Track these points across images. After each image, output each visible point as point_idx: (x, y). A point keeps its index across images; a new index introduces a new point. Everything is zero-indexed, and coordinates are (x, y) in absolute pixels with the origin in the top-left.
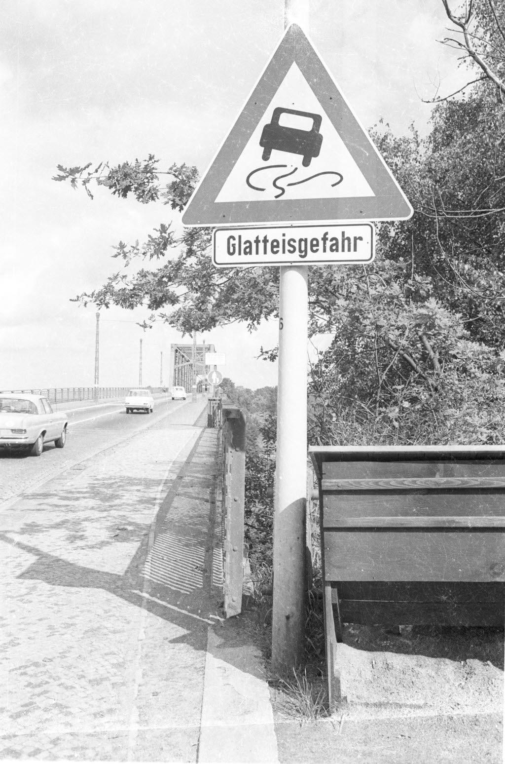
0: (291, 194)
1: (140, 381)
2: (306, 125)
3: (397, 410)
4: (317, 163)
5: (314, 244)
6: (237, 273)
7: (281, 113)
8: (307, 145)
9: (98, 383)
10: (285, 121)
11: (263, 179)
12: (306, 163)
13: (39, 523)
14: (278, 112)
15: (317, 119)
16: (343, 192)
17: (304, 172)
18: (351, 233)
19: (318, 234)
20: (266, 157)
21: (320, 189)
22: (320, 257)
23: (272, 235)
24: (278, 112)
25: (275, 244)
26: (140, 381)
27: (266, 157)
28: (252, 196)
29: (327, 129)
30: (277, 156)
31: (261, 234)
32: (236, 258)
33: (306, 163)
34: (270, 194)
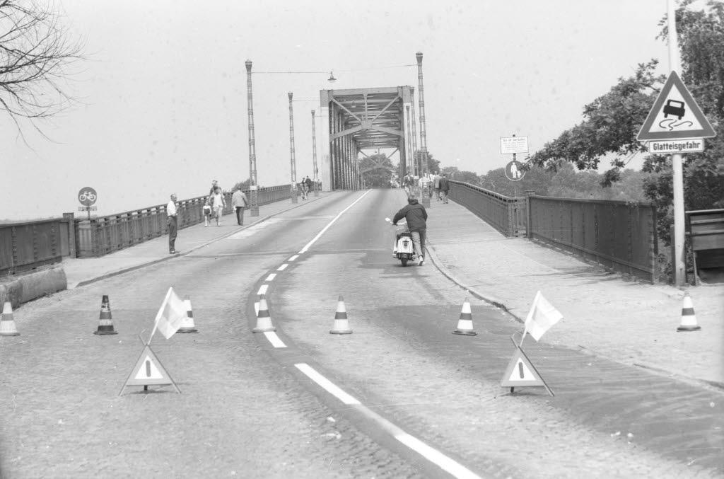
0: (675, 129)
1: (294, 172)
2: (679, 105)
3: (580, 159)
4: (684, 119)
5: (684, 146)
6: (706, 111)
7: (637, 172)
8: (680, 112)
9: (369, 110)
10: (672, 104)
11: (665, 124)
12: (680, 118)
13: (585, 286)
14: (669, 101)
15: (683, 104)
16: (692, 128)
17: (679, 122)
18: (696, 142)
19: (685, 142)
20: (666, 116)
21: (685, 127)
22: (686, 150)
23: (669, 143)
24: (669, 101)
25: (670, 146)
26: (294, 172)
27: (666, 116)
28: (662, 130)
29: (686, 107)
30: (670, 116)
31: (665, 143)
32: (657, 151)
33: (680, 118)
34: (668, 129)
